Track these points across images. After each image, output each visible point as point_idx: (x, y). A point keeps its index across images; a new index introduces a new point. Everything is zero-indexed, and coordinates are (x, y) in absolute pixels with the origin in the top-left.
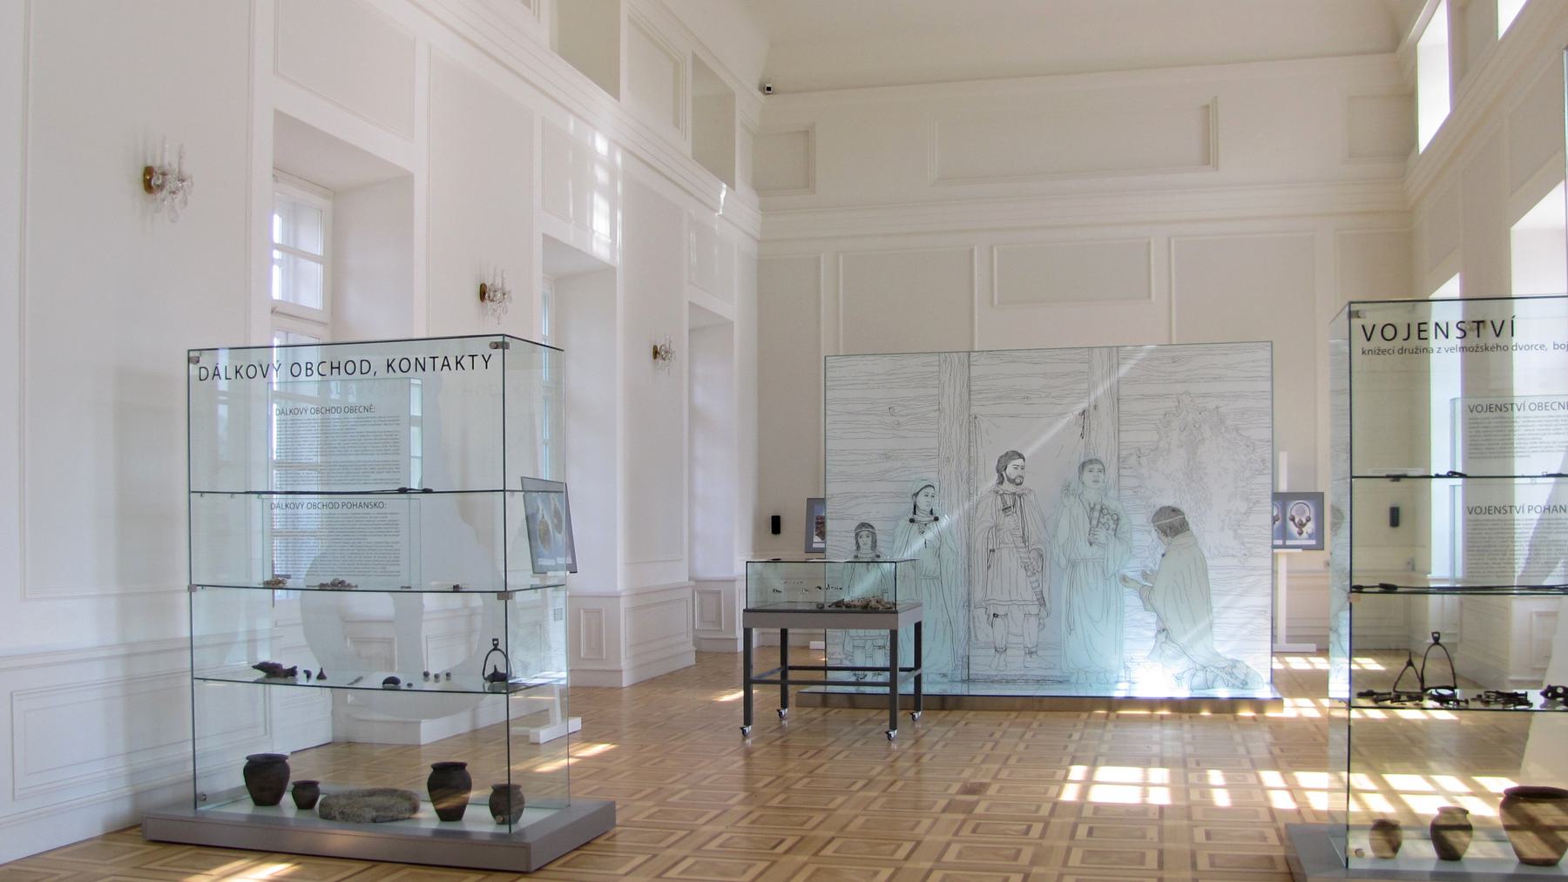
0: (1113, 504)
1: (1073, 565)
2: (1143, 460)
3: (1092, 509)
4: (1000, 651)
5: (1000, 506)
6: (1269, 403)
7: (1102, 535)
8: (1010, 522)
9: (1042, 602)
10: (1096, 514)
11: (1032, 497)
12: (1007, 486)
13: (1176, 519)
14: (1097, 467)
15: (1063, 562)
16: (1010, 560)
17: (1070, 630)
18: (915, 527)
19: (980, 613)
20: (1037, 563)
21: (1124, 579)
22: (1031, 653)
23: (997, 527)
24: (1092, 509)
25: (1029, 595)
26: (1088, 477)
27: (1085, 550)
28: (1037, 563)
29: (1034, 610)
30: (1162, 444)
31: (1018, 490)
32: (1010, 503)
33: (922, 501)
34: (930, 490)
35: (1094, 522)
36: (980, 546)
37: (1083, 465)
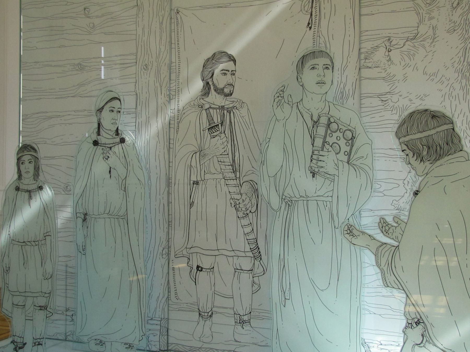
0: (345, 115)
1: (289, 203)
2: (395, 55)
3: (316, 123)
4: (206, 315)
5: (206, 125)
6: (450, 265)
7: (329, 161)
8: (218, 144)
9: (256, 254)
10: (321, 131)
11: (244, 112)
12: (215, 99)
13: (436, 132)
14: (321, 61)
15: (275, 201)
16: (215, 199)
17: (285, 297)
18: (99, 150)
19: (181, 265)
20: (249, 203)
21: (350, 231)
22: (242, 322)
23: (201, 152)
24: (316, 123)
25: (241, 244)
26: (309, 77)
27: (306, 184)
28: (249, 203)
29: (246, 264)
30: (423, 29)
31: (226, 103)
32: (217, 119)
33: (106, 117)
34: (116, 104)
35: (319, 142)
36: (180, 176)
37: (303, 60)
